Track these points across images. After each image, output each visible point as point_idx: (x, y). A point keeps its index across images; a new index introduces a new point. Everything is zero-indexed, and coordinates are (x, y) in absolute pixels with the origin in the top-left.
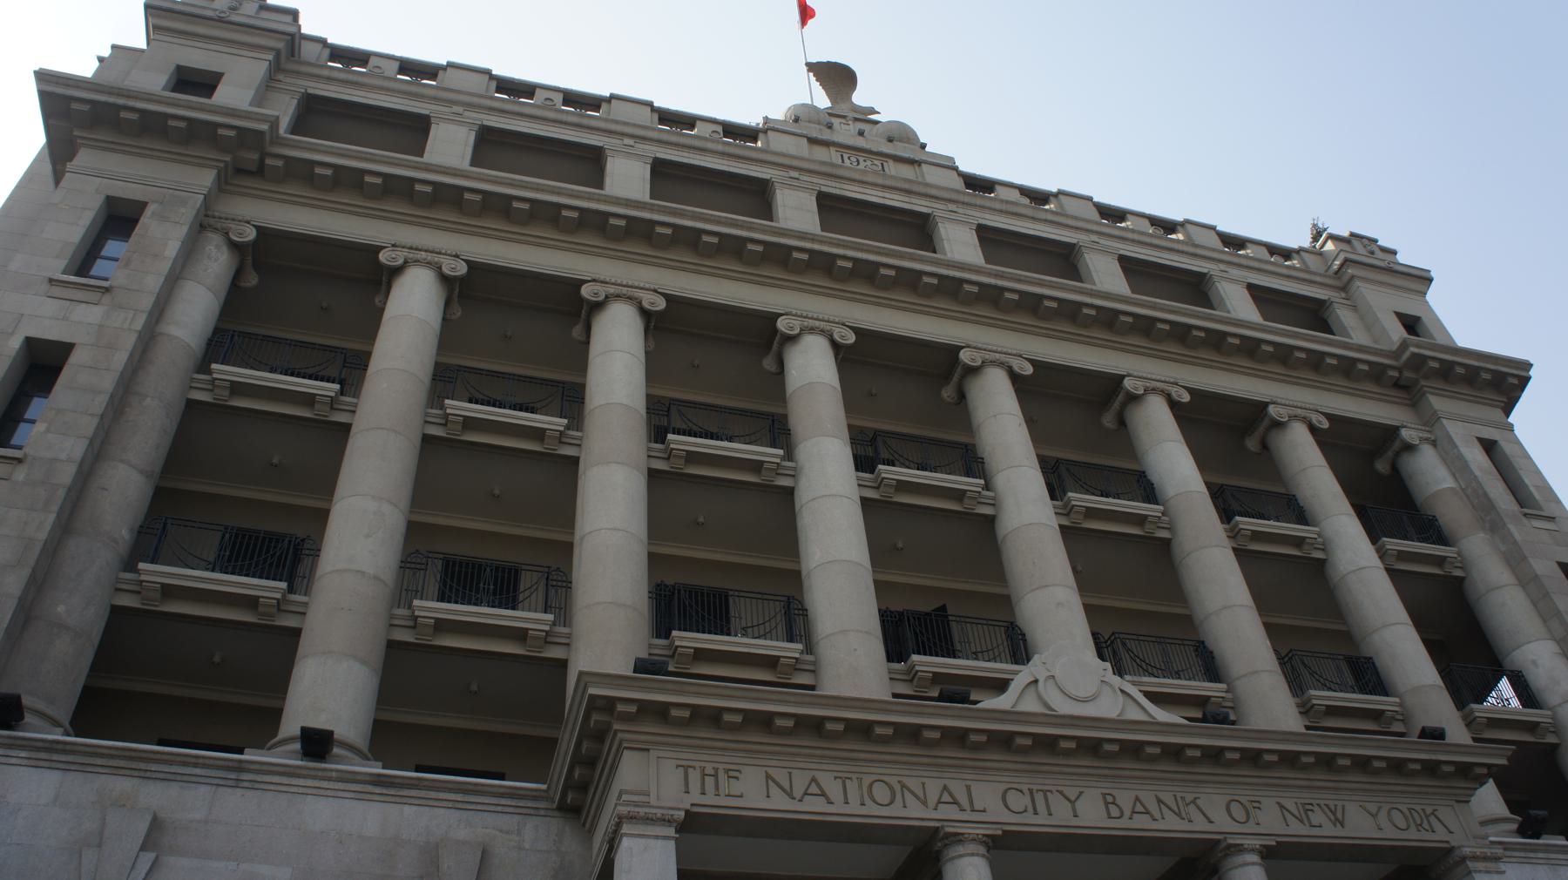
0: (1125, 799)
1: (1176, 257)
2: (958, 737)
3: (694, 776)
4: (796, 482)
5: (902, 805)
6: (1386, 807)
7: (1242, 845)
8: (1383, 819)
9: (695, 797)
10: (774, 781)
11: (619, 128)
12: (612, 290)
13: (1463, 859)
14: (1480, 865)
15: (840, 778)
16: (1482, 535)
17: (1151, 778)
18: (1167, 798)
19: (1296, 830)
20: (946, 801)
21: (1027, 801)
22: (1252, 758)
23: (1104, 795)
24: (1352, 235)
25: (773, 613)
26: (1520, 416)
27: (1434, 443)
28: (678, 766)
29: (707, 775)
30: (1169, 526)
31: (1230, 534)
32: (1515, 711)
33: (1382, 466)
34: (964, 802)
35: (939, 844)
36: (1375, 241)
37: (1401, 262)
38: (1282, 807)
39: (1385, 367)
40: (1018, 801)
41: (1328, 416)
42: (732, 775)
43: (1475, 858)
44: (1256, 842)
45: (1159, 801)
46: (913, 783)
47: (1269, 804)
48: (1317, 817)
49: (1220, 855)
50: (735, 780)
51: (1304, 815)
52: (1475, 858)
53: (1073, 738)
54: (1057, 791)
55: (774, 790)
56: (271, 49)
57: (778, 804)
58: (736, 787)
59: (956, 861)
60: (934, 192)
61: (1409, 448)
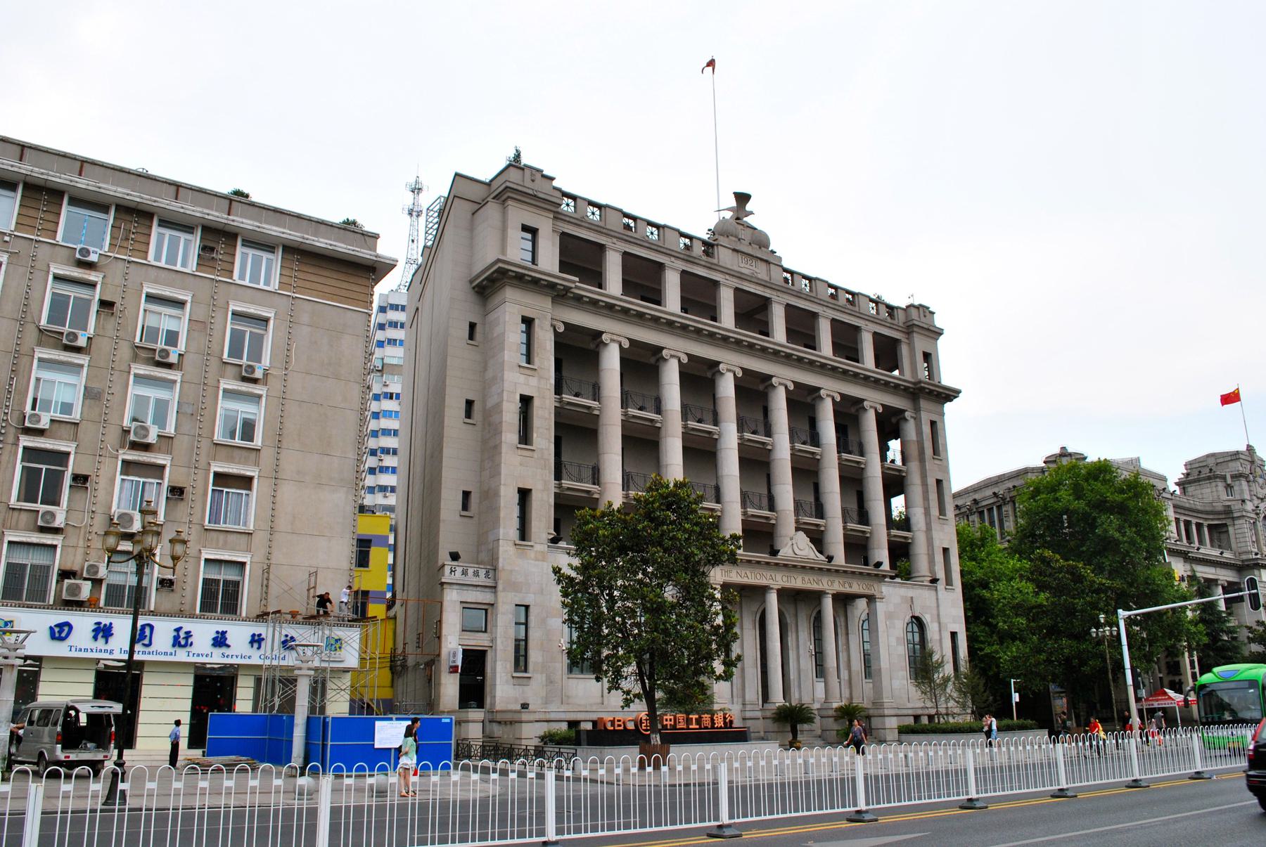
1: (852, 318)
4: (720, 437)
9: (724, 578)
11: (668, 252)
22: (837, 571)
24: (921, 305)
25: (435, 210)
27: (915, 419)
32: (899, 466)
33: (894, 420)
36: (928, 308)
39: (909, 387)
40: (785, 579)
41: (883, 405)
42: (731, 572)
44: (832, 592)
47: (837, 583)
51: (843, 586)
61: (906, 420)
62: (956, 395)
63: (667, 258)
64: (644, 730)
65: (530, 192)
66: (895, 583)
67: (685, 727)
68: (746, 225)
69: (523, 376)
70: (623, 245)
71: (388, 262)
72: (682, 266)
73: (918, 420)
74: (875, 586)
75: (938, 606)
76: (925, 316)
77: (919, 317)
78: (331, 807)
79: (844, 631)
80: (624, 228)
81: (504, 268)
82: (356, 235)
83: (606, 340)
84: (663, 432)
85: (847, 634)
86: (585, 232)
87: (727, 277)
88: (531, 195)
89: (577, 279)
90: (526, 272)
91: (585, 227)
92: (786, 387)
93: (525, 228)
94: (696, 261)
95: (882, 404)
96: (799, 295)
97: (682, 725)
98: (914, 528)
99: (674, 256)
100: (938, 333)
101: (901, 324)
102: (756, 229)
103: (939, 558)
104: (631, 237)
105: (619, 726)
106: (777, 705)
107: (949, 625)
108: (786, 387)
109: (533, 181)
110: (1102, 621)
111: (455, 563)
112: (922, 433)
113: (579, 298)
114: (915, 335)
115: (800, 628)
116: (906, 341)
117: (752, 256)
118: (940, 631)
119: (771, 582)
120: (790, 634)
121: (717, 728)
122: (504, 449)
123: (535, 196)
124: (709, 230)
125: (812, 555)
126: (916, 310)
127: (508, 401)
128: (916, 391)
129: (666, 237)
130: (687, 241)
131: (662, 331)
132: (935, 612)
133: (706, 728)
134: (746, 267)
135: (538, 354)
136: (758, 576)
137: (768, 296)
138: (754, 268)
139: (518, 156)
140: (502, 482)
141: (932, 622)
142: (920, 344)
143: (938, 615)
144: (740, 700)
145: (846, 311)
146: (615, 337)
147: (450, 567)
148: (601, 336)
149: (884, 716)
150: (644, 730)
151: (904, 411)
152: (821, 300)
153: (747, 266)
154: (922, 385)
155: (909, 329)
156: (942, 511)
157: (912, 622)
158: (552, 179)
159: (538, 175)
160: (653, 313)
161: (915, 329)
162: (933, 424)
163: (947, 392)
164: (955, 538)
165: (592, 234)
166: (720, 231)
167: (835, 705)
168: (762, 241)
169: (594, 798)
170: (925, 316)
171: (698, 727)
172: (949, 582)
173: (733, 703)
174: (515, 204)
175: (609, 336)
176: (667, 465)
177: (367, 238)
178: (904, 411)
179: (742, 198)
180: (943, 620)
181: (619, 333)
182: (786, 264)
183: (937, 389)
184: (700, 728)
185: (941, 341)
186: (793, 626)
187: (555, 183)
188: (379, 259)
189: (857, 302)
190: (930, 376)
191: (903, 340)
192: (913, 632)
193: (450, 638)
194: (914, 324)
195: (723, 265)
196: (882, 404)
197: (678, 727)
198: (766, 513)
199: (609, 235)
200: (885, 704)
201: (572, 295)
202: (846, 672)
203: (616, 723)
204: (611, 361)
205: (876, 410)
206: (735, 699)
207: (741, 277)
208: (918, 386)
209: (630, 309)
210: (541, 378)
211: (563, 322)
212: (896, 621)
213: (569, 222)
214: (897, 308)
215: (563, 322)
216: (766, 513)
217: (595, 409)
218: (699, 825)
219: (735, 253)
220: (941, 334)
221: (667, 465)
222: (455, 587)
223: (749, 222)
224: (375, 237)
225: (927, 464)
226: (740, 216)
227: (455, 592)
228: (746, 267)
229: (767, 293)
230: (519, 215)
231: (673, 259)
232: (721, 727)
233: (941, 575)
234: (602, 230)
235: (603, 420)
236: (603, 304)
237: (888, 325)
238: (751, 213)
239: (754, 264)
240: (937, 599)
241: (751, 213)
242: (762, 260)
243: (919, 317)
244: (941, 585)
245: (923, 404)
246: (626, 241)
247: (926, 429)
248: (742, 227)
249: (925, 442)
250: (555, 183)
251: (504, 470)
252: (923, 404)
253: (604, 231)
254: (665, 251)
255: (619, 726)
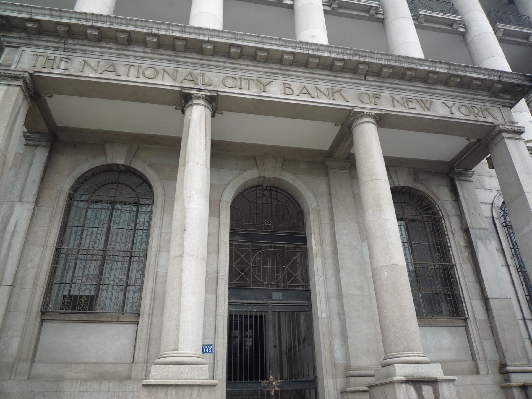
0: (296, 86)
5: (161, 79)
6: (457, 104)
7: (363, 112)
10: (167, 73)
13: (501, 131)
15: (247, 79)
17: (306, 77)
18: (398, 97)
20: (304, 92)
23: (284, 84)
28: (126, 65)
30: (383, 13)
31: (413, 18)
35: (351, 119)
38: (393, 99)
43: (507, 131)
45: (318, 89)
48: (133, 71)
49: (351, 119)
50: (411, 102)
52: (507, 131)
54: (415, 99)
55: (396, 104)
57: (142, 80)
59: (361, 125)
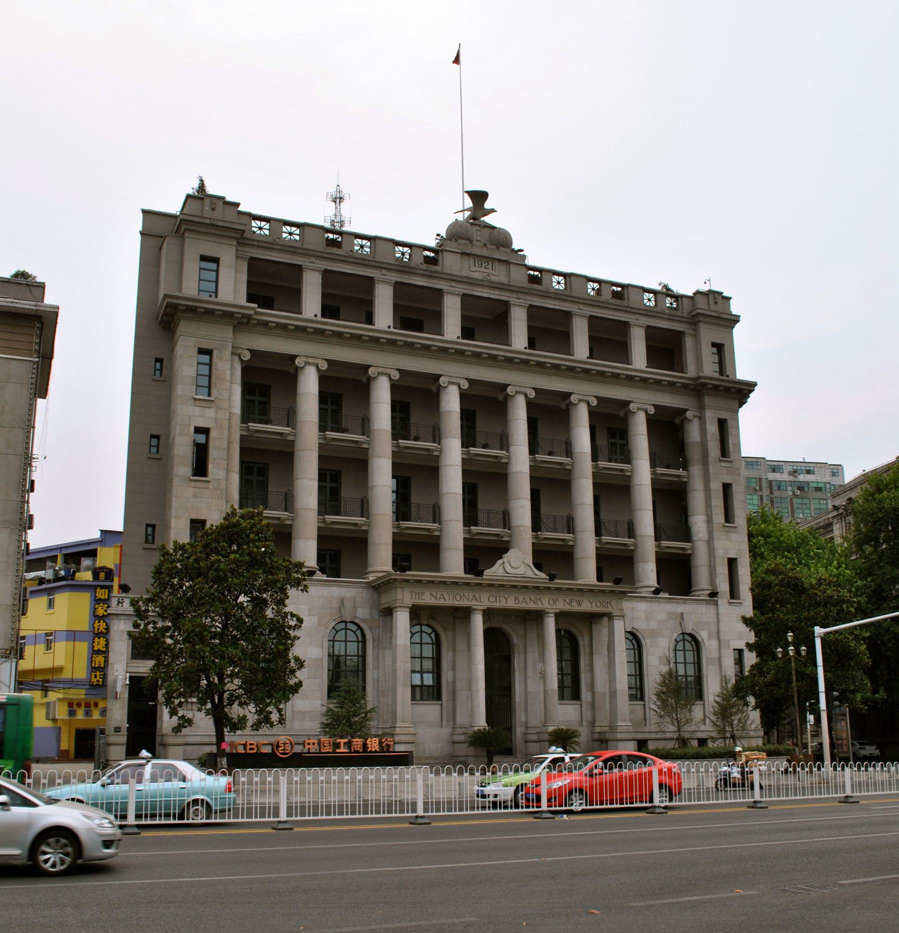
0: (521, 598)
2: (480, 584)
3: (414, 594)
4: (441, 454)
8: (594, 605)
12: (380, 370)
14: (618, 618)
16: (700, 466)
19: (567, 608)
21: (494, 599)
26: (744, 413)
27: (700, 418)
29: (425, 658)
34: (478, 599)
37: (733, 313)
46: (466, 595)
53: (565, 365)
55: (433, 598)
56: (235, 238)
58: (423, 597)
60: (513, 289)
62: (751, 388)
63: (377, 272)
64: (281, 754)
65: (208, 221)
66: (660, 598)
67: (331, 751)
68: (482, 224)
69: (198, 409)
70: (323, 262)
71: (48, 309)
72: (394, 277)
73: (702, 418)
74: (613, 603)
75: (718, 622)
76: (716, 303)
77: (708, 304)
78: (136, 802)
79: (587, 649)
80: (327, 245)
81: (172, 303)
82: (21, 287)
83: (575, 401)
84: (298, 446)
85: (592, 654)
86: (277, 255)
87: (453, 284)
88: (209, 224)
89: (256, 305)
90: (198, 304)
91: (278, 250)
92: (526, 396)
93: (714, 345)
94: (413, 271)
95: (654, 405)
96: (547, 294)
97: (327, 749)
98: (695, 538)
99: (386, 269)
100: (735, 320)
101: (685, 315)
102: (494, 228)
103: (722, 571)
104: (331, 254)
105: (251, 749)
106: (476, 729)
107: (731, 642)
108: (526, 396)
109: (213, 209)
110: (790, 639)
111: (124, 595)
112: (706, 434)
113: (265, 324)
114: (701, 325)
115: (529, 649)
116: (693, 332)
117: (487, 258)
118: (720, 649)
119: (474, 602)
120: (516, 655)
121: (371, 752)
122: (176, 481)
123: (213, 225)
124: (438, 235)
125: (529, 573)
126: (705, 297)
127: (181, 435)
128: (698, 388)
129: (377, 248)
130: (596, 286)
131: (549, 374)
132: (714, 628)
133: (357, 752)
134: (477, 272)
135: (216, 386)
136: (458, 597)
137: (506, 299)
138: (490, 271)
139: (202, 187)
140: (173, 515)
141: (709, 638)
142: (708, 335)
143: (718, 632)
144: (451, 724)
145: (609, 306)
146: (311, 360)
147: (117, 599)
148: (629, 405)
149: (618, 740)
150: (281, 754)
151: (685, 410)
152: (574, 297)
153: (482, 269)
154: (702, 380)
155: (694, 320)
156: (728, 517)
157: (684, 640)
158: (238, 205)
159: (220, 203)
160: (472, 349)
161: (701, 319)
162: (722, 424)
163: (738, 386)
164: (745, 547)
165: (286, 256)
166: (456, 234)
167: (551, 729)
168: (501, 240)
169: (631, 777)
170: (716, 303)
171: (346, 751)
172: (734, 593)
173: (442, 727)
174: (193, 236)
175: (304, 359)
176: (372, 487)
177: (32, 288)
178: (685, 410)
179: (478, 197)
180: (724, 636)
181: (316, 355)
182: (530, 262)
183: (723, 384)
184: (350, 752)
185: (737, 330)
186: (522, 647)
187: (240, 209)
188: (38, 308)
189: (440, 260)
190: (722, 371)
191: (687, 331)
192: (684, 650)
193: (116, 667)
194: (698, 314)
195: (448, 272)
196: (654, 405)
197: (322, 751)
198: (626, 540)
199: (306, 255)
200: (619, 728)
201: (256, 322)
202: (589, 695)
203: (249, 747)
204: (451, 403)
205: (646, 413)
206: (445, 723)
207: (470, 282)
208: (699, 382)
209: (575, 367)
210: (218, 408)
211: (248, 349)
212: (660, 640)
213: (258, 246)
214: (682, 296)
215: (248, 349)
216: (626, 540)
217: (567, 464)
218: (742, 800)
219: (465, 258)
220: (738, 321)
221: (372, 487)
222: (122, 617)
223: (486, 221)
224: (42, 286)
225: (711, 467)
226: (476, 216)
227: (122, 622)
228: (477, 272)
229: (504, 297)
230: (196, 247)
231: (384, 272)
232: (376, 752)
233: (723, 586)
234: (297, 250)
235: (576, 473)
236: (518, 361)
237: (668, 317)
238: (493, 211)
239: (490, 264)
240: (718, 614)
241: (493, 211)
242: (499, 260)
243: (708, 304)
244: (723, 600)
245: (708, 400)
246: (326, 258)
247: (712, 429)
248: (478, 228)
249: (709, 443)
250: (240, 209)
251: (175, 503)
252: (708, 400)
253: (300, 251)
254: (373, 264)
255: (251, 749)
